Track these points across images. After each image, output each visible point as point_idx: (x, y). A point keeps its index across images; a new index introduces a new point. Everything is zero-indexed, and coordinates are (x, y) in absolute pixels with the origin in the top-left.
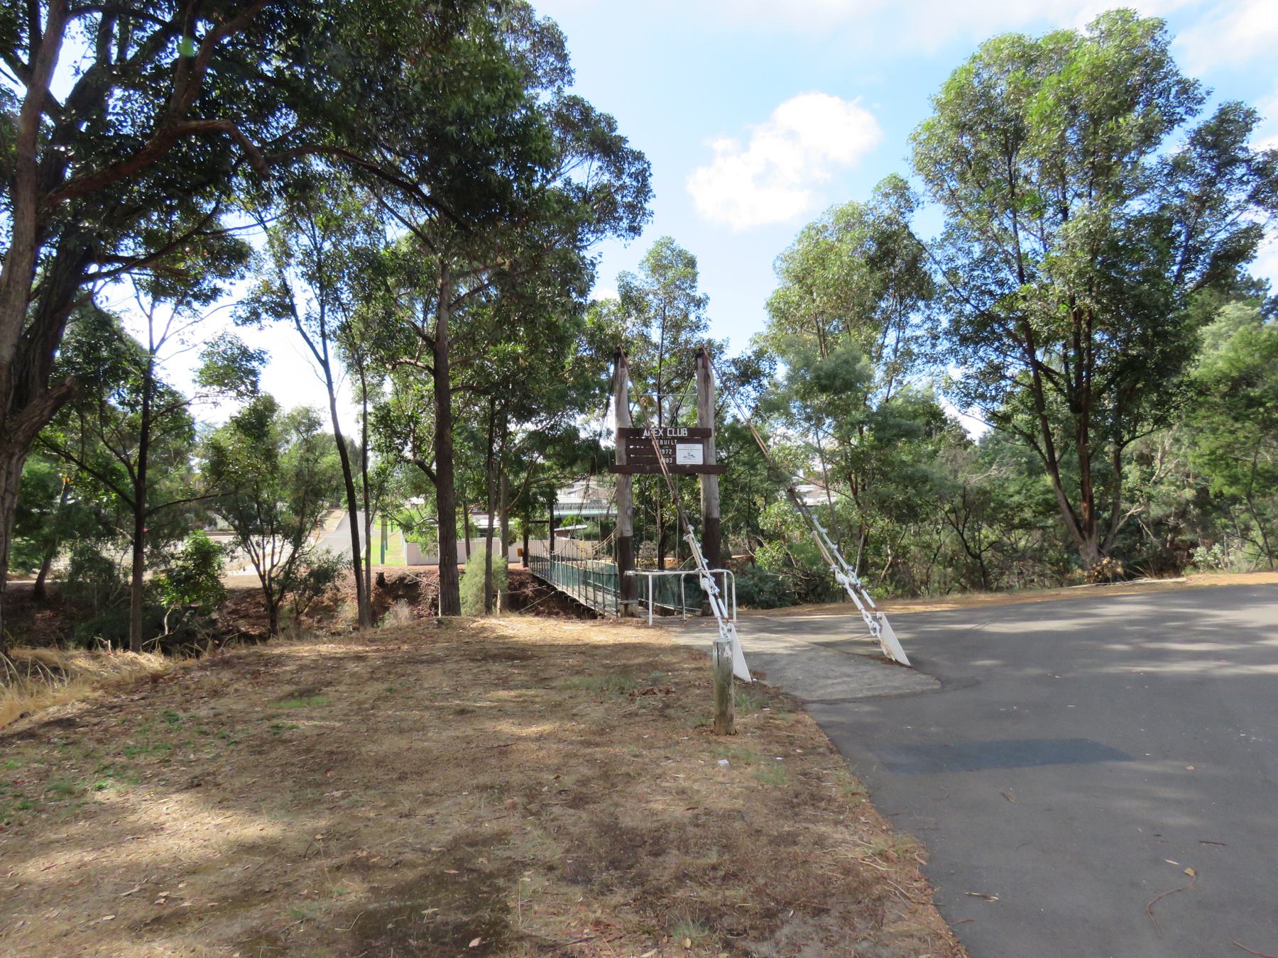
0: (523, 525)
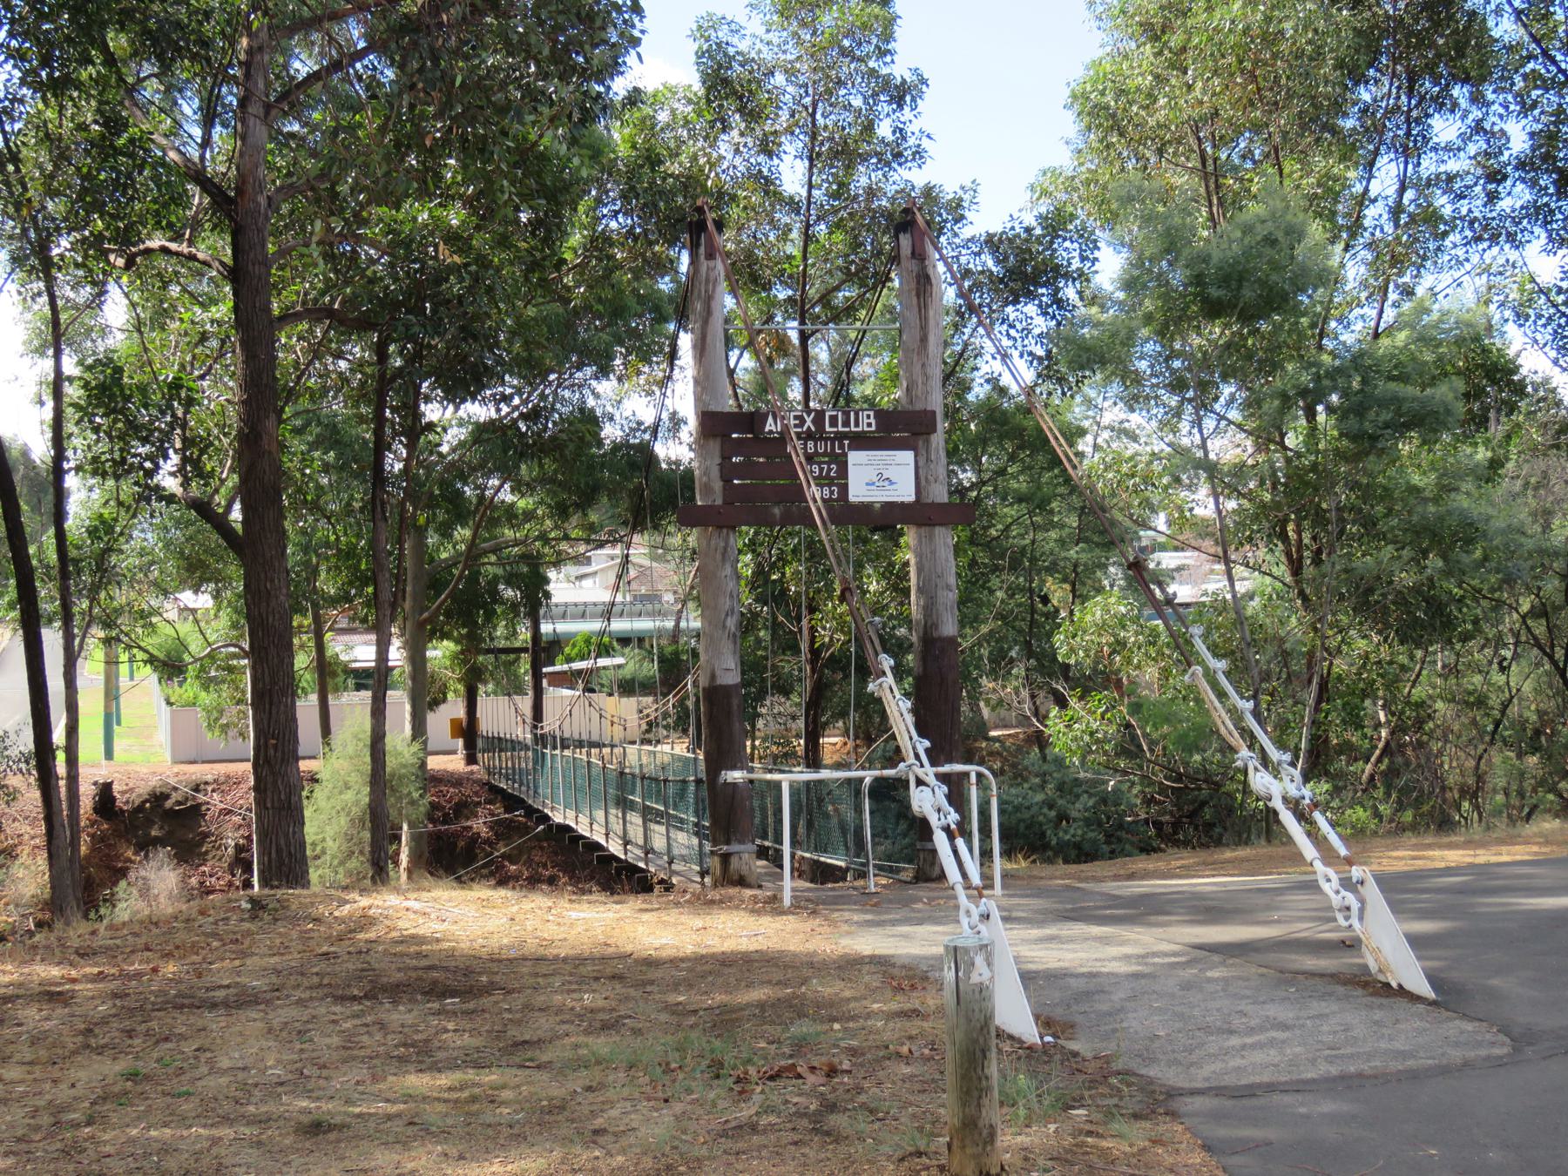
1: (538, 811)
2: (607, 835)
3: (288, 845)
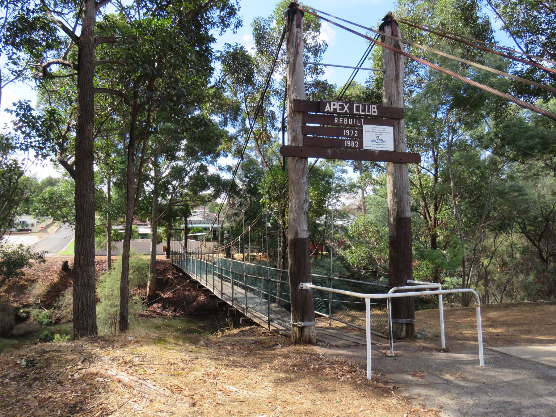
0: (166, 231)
1: (187, 274)
2: (213, 289)
3: (87, 301)
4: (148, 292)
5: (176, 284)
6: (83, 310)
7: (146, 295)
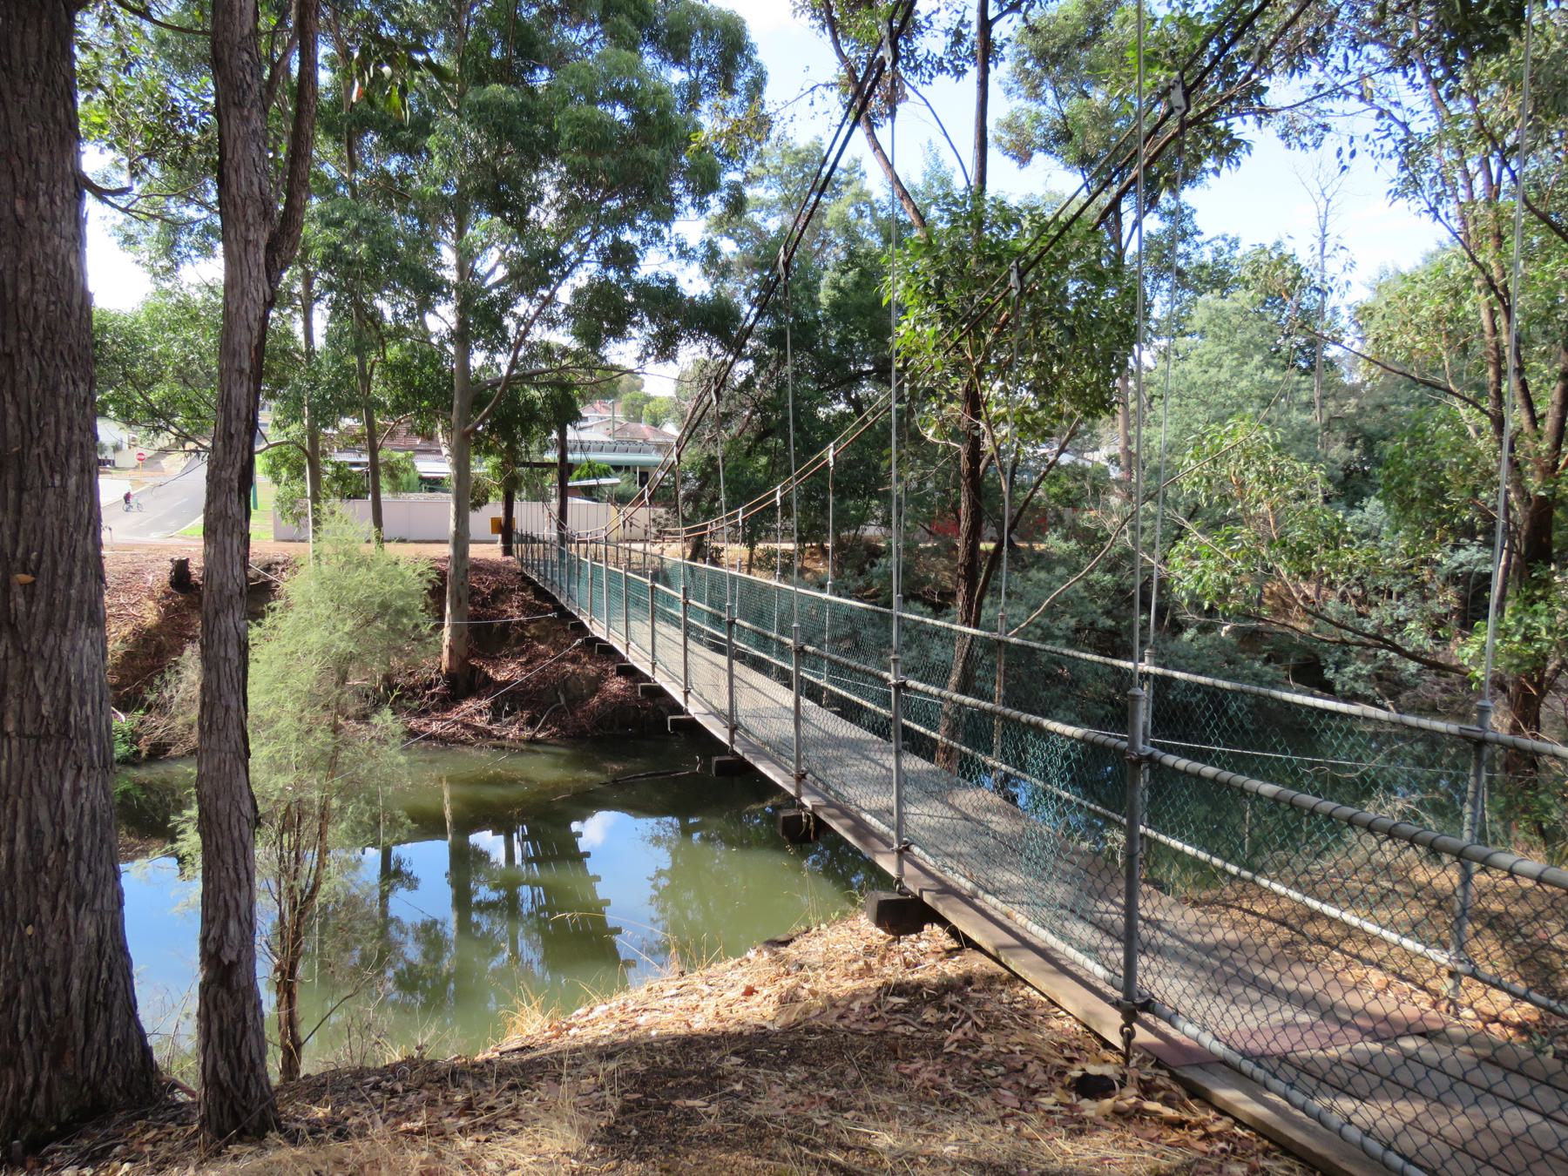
0: (502, 469)
1: (574, 617)
2: (654, 665)
3: (58, 821)
4: (445, 664)
5: (533, 637)
6: (38, 866)
7: (439, 671)
